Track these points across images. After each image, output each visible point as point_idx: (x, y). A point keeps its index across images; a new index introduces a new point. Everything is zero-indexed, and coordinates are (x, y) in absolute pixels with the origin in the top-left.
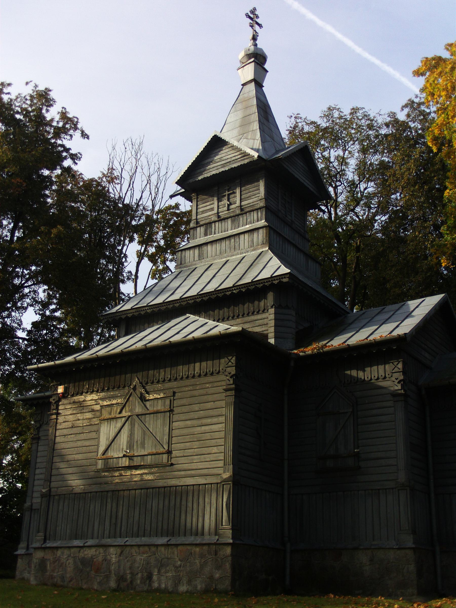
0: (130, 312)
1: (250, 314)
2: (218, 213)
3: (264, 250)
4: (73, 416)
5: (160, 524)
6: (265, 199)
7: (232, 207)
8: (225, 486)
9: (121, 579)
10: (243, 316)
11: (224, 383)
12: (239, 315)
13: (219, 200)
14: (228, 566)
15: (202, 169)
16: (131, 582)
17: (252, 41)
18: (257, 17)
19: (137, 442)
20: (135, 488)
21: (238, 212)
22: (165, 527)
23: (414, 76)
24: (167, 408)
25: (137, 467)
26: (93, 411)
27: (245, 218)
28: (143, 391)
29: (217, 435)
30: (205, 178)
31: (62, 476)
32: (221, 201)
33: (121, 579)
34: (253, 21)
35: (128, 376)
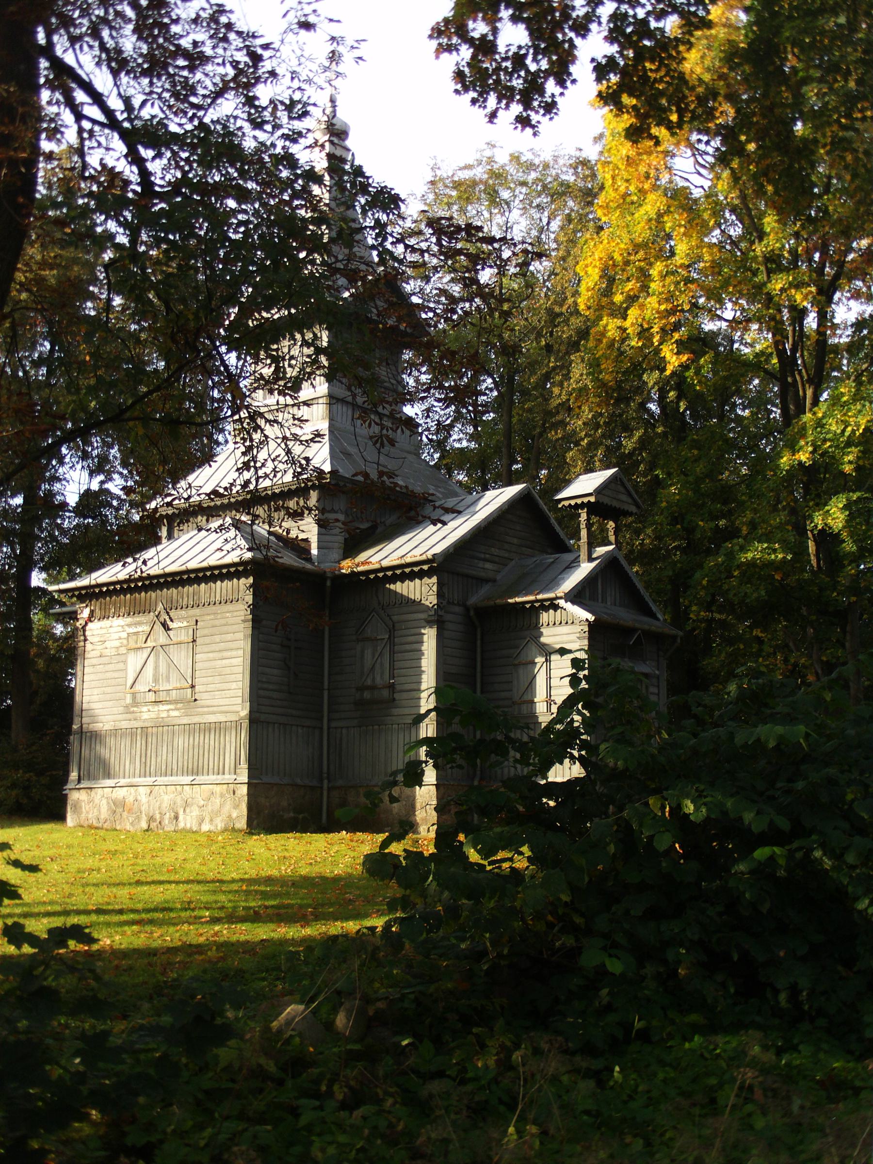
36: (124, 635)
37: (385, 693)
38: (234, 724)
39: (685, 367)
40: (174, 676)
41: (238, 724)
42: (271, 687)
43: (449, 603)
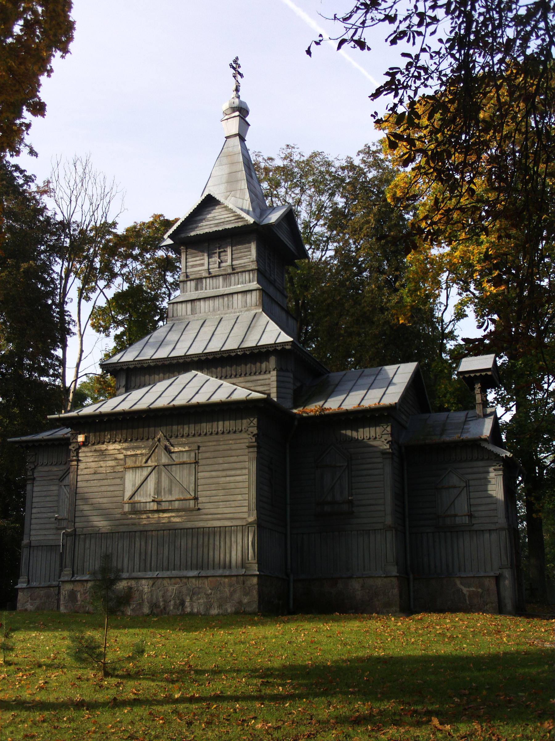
0: (132, 363)
1: (252, 374)
2: (209, 269)
3: (257, 311)
4: (95, 463)
5: (189, 560)
6: (257, 261)
7: (223, 265)
8: (250, 528)
9: (154, 606)
10: (245, 375)
11: (245, 441)
12: (241, 374)
13: (210, 257)
14: (255, 593)
15: (194, 226)
16: (165, 608)
17: (235, 92)
18: (239, 67)
19: (164, 489)
20: (163, 529)
21: (230, 271)
22: (194, 562)
23: (376, 128)
24: (193, 460)
25: (164, 511)
26: (116, 459)
27: (237, 277)
28: (168, 444)
29: (241, 485)
30: (197, 235)
31: (87, 518)
32: (211, 258)
33: (154, 606)
34: (236, 71)
35: (152, 429)
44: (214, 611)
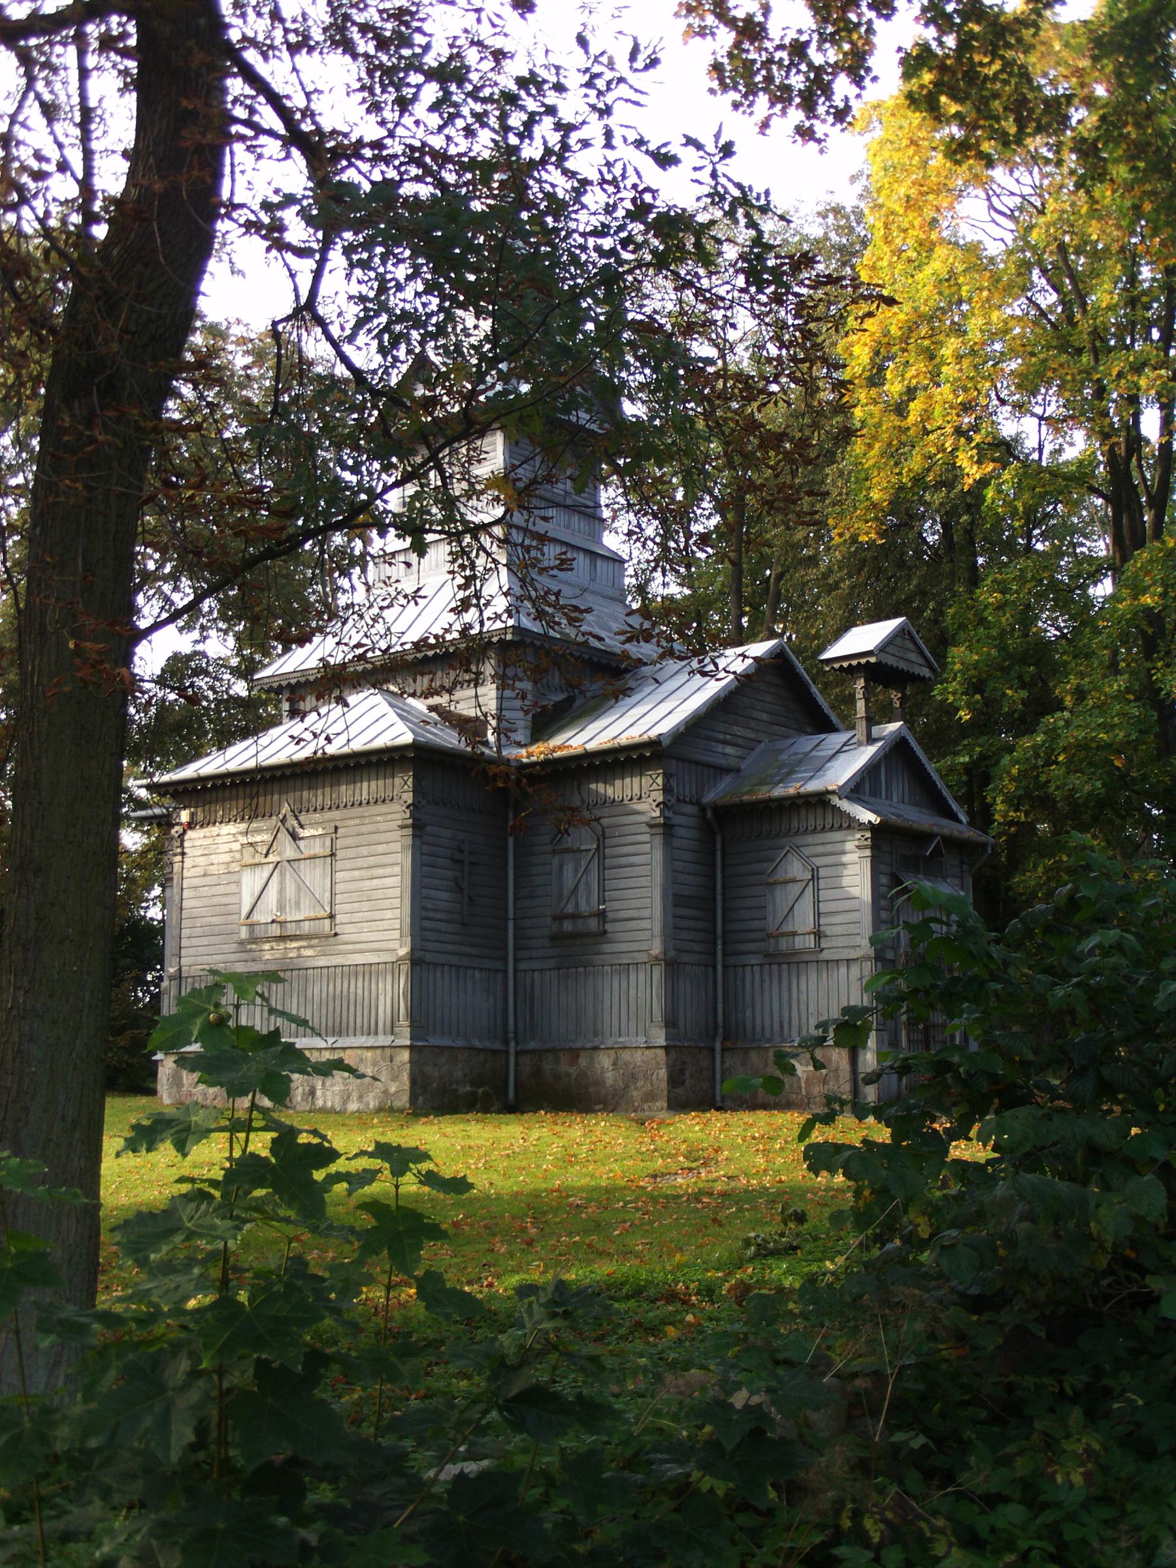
36: (236, 846)
37: (593, 924)
38: (389, 967)
39: (983, 483)
40: (305, 902)
41: (395, 964)
42: (439, 916)
43: (678, 800)
44: (353, 1106)
